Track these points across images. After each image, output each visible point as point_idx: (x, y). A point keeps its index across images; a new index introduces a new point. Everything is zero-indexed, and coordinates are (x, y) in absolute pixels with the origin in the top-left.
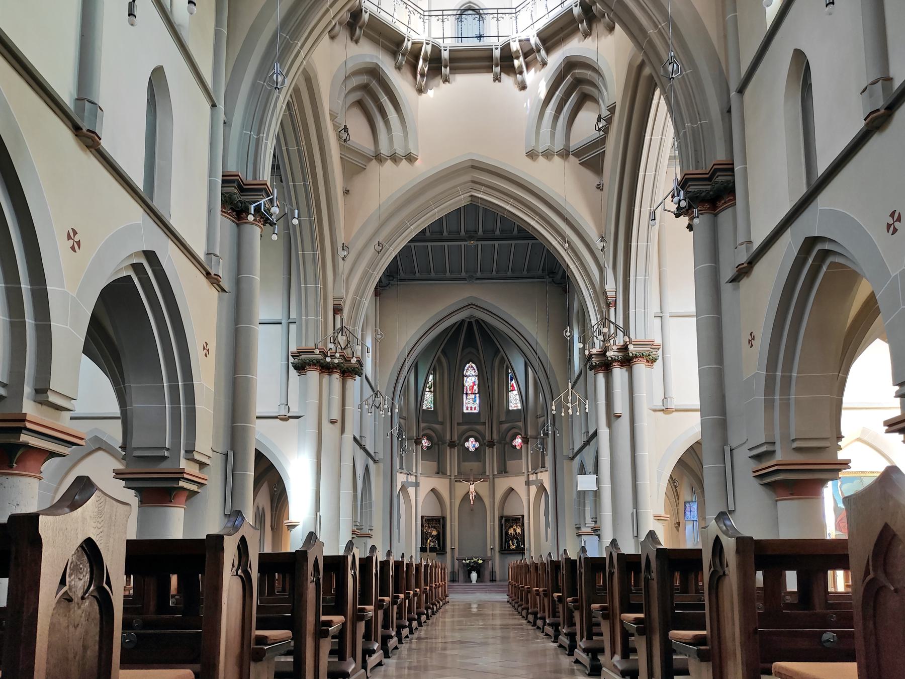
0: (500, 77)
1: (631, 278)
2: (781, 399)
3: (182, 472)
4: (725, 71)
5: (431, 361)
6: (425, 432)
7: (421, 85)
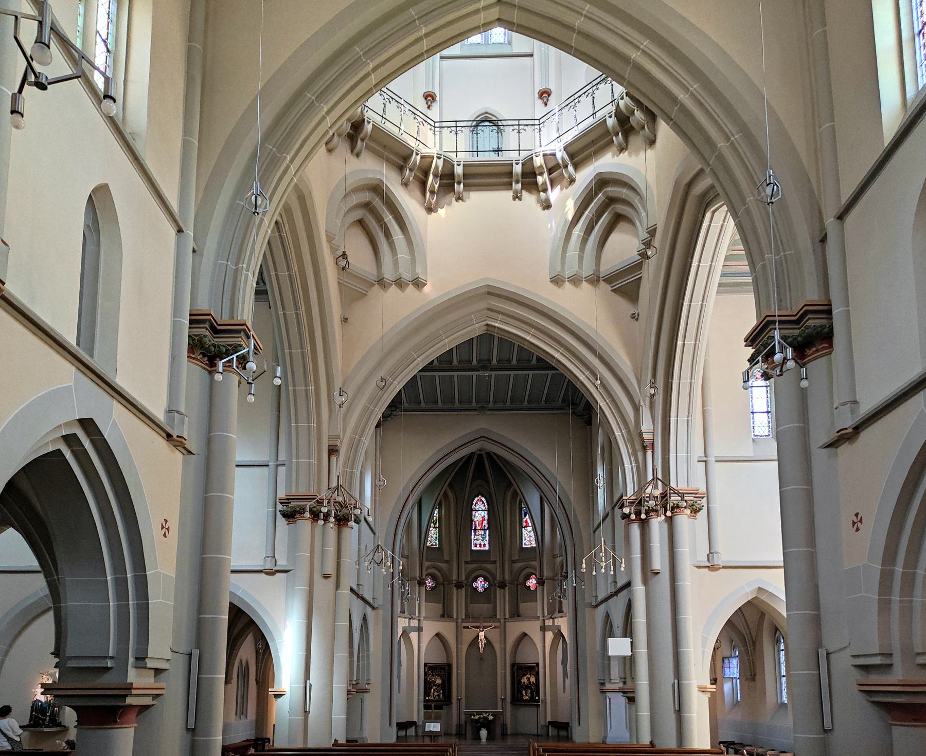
0: (521, 196)
1: (672, 419)
2: (901, 602)
3: (130, 687)
4: (816, 192)
5: (436, 496)
6: (430, 571)
7: (431, 203)
